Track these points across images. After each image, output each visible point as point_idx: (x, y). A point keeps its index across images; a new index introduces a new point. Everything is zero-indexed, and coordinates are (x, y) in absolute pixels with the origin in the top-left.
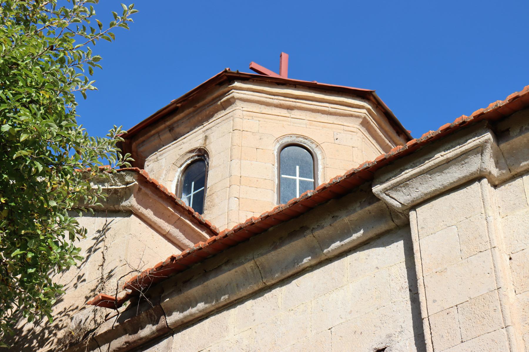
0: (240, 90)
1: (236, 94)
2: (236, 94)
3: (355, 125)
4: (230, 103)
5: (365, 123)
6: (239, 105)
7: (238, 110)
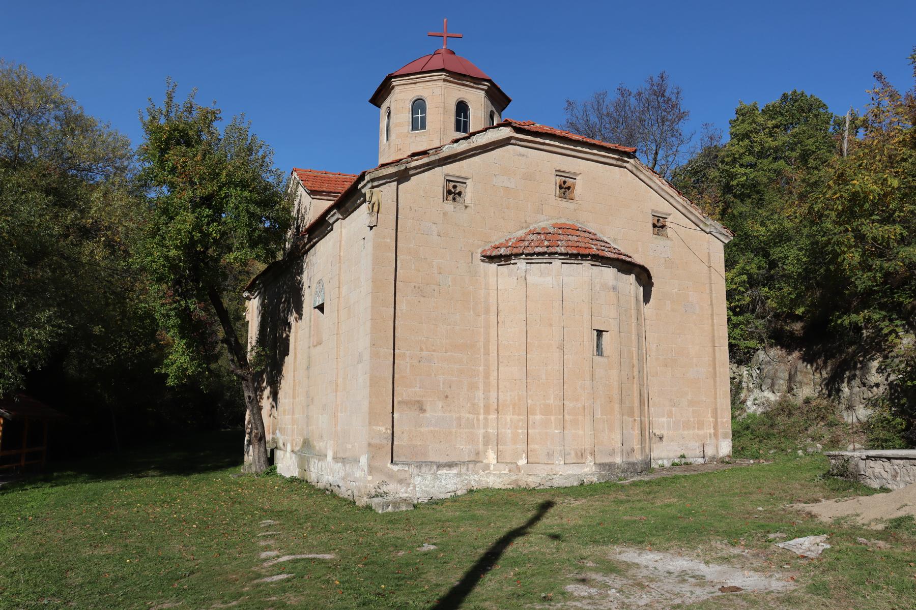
0: (395, 82)
1: (394, 84)
2: (394, 84)
3: (441, 83)
4: (393, 87)
5: (445, 80)
6: (396, 88)
7: (397, 90)
